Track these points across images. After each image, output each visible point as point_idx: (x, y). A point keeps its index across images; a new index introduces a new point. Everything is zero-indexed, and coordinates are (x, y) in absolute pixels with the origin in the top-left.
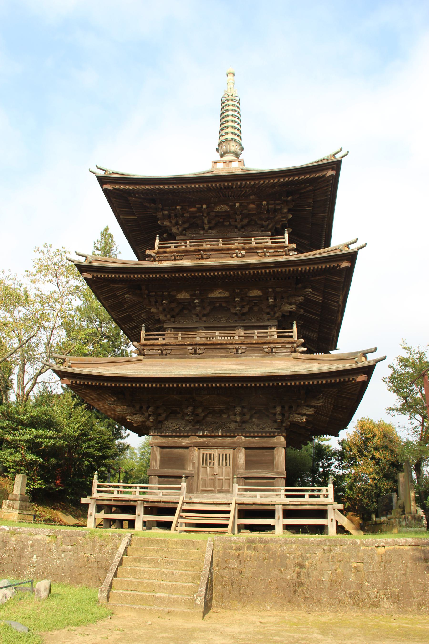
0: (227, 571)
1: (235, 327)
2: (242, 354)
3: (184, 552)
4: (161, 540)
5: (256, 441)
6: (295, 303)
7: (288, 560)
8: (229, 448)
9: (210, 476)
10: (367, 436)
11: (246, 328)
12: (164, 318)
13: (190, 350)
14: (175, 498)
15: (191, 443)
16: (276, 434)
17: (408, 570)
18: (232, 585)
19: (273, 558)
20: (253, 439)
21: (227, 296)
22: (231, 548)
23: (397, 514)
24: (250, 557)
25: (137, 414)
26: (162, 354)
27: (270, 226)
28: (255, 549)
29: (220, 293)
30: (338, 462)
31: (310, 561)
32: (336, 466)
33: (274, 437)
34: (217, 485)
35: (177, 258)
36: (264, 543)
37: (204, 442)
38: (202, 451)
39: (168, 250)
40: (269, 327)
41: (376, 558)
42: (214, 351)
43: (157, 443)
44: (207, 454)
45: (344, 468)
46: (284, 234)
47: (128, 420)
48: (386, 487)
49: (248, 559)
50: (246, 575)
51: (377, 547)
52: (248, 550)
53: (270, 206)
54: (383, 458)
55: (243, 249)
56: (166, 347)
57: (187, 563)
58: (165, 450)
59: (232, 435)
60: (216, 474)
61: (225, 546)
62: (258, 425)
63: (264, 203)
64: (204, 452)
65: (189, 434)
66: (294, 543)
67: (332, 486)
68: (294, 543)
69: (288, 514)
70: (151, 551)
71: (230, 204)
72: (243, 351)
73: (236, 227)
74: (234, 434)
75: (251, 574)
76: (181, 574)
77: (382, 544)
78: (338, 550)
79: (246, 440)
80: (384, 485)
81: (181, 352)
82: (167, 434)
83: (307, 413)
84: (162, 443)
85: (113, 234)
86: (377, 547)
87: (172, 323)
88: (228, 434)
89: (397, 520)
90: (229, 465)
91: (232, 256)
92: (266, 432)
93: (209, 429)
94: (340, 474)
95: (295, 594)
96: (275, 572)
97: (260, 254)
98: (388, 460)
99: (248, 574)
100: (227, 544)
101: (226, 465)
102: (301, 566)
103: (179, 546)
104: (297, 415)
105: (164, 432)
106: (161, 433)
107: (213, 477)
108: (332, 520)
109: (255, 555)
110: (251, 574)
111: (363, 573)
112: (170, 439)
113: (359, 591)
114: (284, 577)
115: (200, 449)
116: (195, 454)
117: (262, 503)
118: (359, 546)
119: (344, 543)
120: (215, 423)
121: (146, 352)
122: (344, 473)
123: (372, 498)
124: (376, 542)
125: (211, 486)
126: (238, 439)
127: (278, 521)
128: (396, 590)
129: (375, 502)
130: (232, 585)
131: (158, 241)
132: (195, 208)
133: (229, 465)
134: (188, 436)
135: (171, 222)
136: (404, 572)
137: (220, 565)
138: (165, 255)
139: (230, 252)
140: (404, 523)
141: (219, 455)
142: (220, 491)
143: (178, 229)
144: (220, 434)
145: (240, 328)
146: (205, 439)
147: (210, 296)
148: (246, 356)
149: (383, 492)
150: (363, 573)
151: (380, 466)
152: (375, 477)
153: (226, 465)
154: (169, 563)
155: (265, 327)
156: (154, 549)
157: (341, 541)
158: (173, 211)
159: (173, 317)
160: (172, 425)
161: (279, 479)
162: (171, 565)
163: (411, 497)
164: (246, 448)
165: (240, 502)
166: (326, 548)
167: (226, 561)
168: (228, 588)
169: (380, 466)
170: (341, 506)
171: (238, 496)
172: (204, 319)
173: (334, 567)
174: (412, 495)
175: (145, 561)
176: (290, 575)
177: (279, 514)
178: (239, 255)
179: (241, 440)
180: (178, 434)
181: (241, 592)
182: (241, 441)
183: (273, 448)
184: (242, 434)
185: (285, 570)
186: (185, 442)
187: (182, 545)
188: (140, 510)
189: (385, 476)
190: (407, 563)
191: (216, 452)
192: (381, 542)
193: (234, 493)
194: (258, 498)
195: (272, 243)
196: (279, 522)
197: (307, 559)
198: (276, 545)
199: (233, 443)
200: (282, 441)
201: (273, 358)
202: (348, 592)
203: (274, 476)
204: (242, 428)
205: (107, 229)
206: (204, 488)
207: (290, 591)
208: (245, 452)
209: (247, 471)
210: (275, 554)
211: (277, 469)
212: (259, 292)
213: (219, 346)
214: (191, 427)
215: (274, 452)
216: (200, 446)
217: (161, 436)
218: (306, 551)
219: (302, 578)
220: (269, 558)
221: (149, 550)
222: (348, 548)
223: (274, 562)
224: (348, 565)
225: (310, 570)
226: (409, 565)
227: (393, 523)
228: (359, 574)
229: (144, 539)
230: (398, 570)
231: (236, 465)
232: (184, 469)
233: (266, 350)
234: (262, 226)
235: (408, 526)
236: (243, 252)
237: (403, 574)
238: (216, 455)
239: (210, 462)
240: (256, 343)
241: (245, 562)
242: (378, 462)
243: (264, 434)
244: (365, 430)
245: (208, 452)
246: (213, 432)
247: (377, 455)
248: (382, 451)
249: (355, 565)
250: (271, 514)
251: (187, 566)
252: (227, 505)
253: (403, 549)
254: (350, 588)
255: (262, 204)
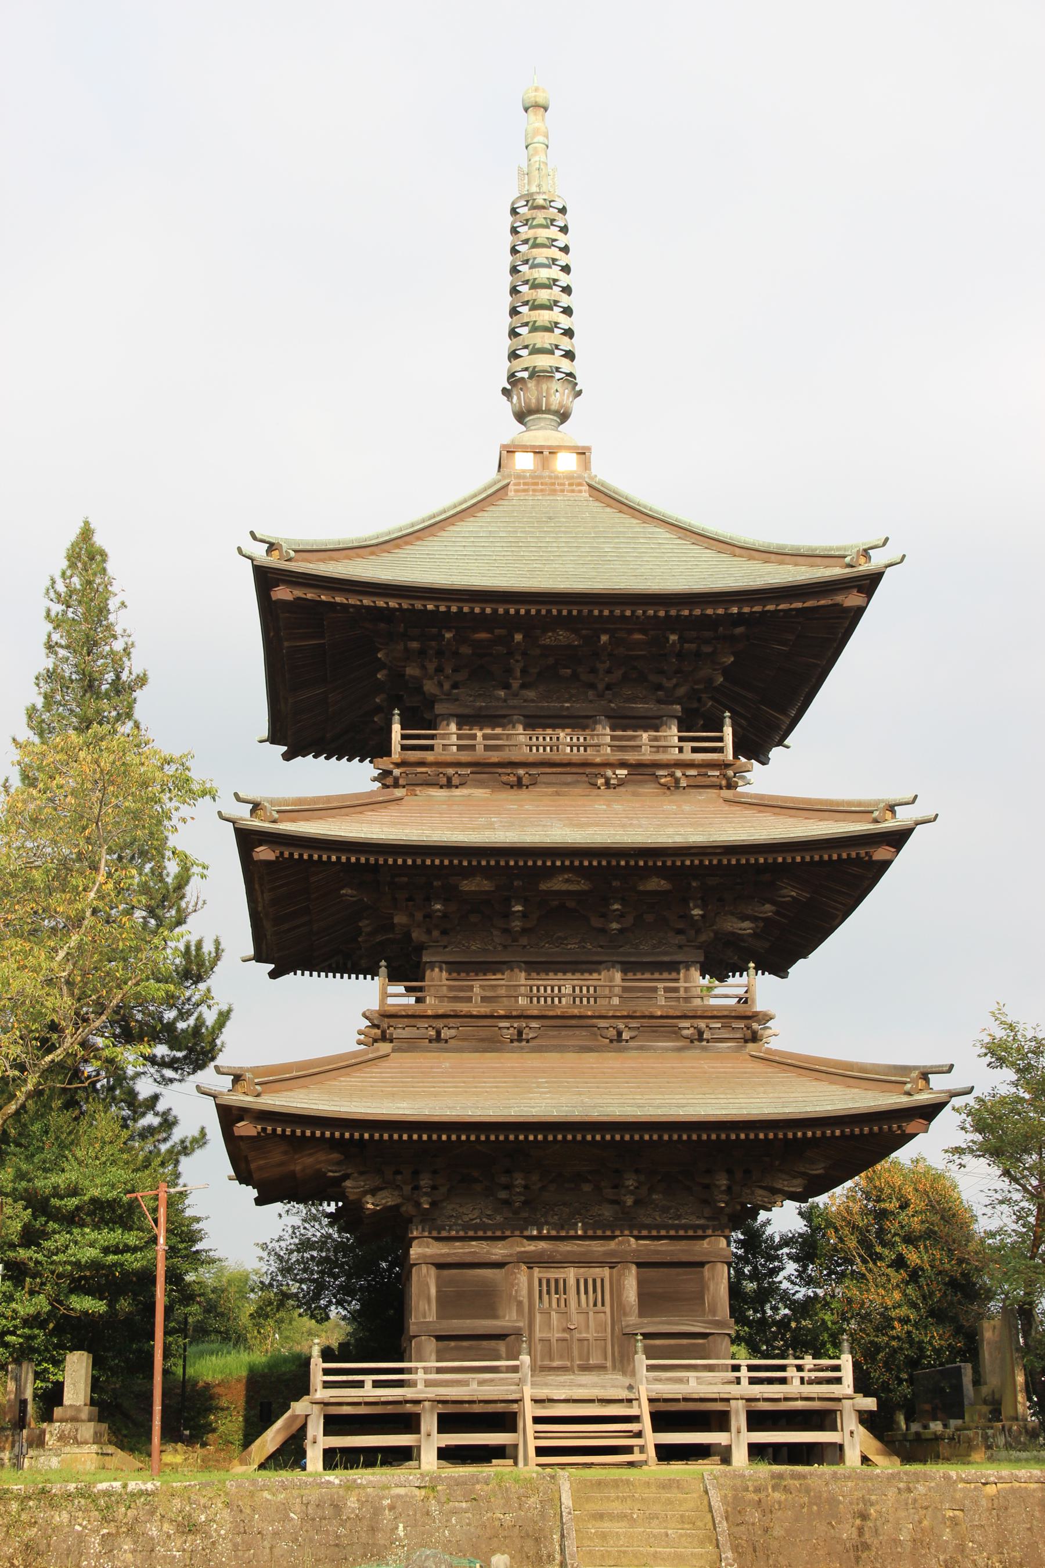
0: (743, 1528)
1: (600, 963)
2: (631, 1044)
3: (669, 1499)
4: (622, 1481)
5: (664, 1248)
6: (754, 919)
7: (841, 1506)
8: (601, 1264)
9: (558, 1332)
10: (886, 1205)
11: (627, 967)
12: (424, 938)
13: (505, 1031)
14: (507, 1390)
15: (511, 1255)
16: (709, 1232)
17: (1035, 1523)
18: (755, 1551)
19: (816, 1504)
20: (656, 1243)
21: (585, 888)
22: (746, 1489)
23: (980, 1418)
24: (780, 1503)
25: (381, 1189)
26: (438, 1038)
27: (681, 691)
28: (786, 1489)
29: (567, 881)
30: (796, 1266)
31: (878, 1507)
32: (793, 1278)
33: (703, 1238)
34: (576, 1353)
35: (456, 781)
36: (799, 1479)
37: (542, 1253)
38: (537, 1272)
39: (429, 756)
40: (681, 966)
41: (984, 1502)
42: (563, 1033)
43: (431, 1256)
44: (548, 1281)
45: (809, 1282)
46: (723, 727)
47: (370, 1206)
48: (937, 1343)
49: (777, 1507)
50: (775, 1534)
51: (984, 1484)
52: (773, 1490)
53: (686, 645)
54: (927, 1267)
55: (623, 765)
56: (446, 1021)
57: (682, 1516)
58: (446, 1272)
59: (608, 1233)
60: (572, 1327)
61: (735, 1485)
62: (665, 1210)
63: (673, 638)
64: (541, 1275)
65: (508, 1233)
66: (849, 1477)
67: (850, 1357)
68: (849, 1477)
69: (758, 1420)
70: (613, 1501)
71: (584, 632)
72: (633, 1034)
73: (592, 686)
74: (613, 1232)
75: (782, 1532)
76: (681, 1536)
77: (992, 1479)
78: (921, 1488)
79: (638, 1245)
80: (933, 1337)
81: (484, 1033)
82: (453, 1233)
83: (786, 1189)
84: (442, 1255)
85: (109, 555)
86: (984, 1484)
87: (441, 949)
88: (599, 1233)
89: (980, 1432)
90: (603, 1305)
91: (593, 781)
92: (685, 1227)
93: (550, 1220)
94: (799, 1296)
95: (858, 1562)
96: (821, 1528)
97: (663, 781)
98: (940, 1273)
99: (778, 1532)
100: (738, 1482)
101: (595, 1305)
102: (864, 1516)
103: (654, 1490)
104: (761, 1192)
105: (444, 1229)
106: (439, 1233)
107: (566, 1335)
108: (852, 1433)
109: (786, 1500)
110: (782, 1532)
111: (964, 1526)
112: (457, 1244)
113: (959, 1557)
114: (837, 1535)
115: (531, 1268)
116: (523, 1281)
117: (702, 1396)
118: (955, 1482)
119: (931, 1477)
120: (564, 1204)
121: (397, 1033)
122: (812, 1295)
123: (899, 1371)
124: (983, 1476)
125: (561, 1358)
126: (620, 1243)
127: (738, 1437)
128: (1017, 1554)
129: (906, 1380)
130: (755, 1551)
131: (399, 726)
132: (492, 633)
133: (603, 1305)
134: (503, 1238)
135: (423, 667)
136: (1028, 1526)
137: (731, 1519)
138: (420, 770)
139: (588, 770)
140: (1001, 1441)
141: (578, 1281)
142: (586, 1368)
143: (440, 685)
144: (580, 1232)
145: (613, 967)
146: (542, 1245)
147: (543, 887)
148: (641, 1048)
149: (930, 1356)
150: (964, 1526)
151: (920, 1287)
152: (908, 1317)
153: (595, 1305)
154: (653, 1518)
155: (673, 967)
156: (618, 1497)
157: (925, 1474)
158: (433, 643)
159: (444, 932)
160: (461, 1210)
161: (719, 1339)
162: (656, 1522)
163: (1018, 1383)
164: (639, 1265)
165: (654, 1395)
166: (902, 1485)
167: (739, 1512)
168: (749, 1558)
169: (920, 1287)
170: (870, 1403)
171: (649, 1384)
172: (524, 941)
173: (916, 1517)
174: (1020, 1379)
175: (612, 1517)
176: (847, 1532)
177: (739, 1420)
178: (612, 782)
179: (629, 1245)
180: (480, 1233)
181: (771, 1562)
182: (628, 1249)
183: (702, 1264)
184: (631, 1232)
185: (839, 1523)
186: (498, 1251)
187: (659, 1486)
188: (429, 1423)
189: (932, 1313)
190: (1033, 1510)
191: (571, 1274)
192: (990, 1475)
193: (638, 1376)
194: (697, 1384)
195: (695, 750)
196: (739, 1439)
197: (872, 1504)
198: (820, 1482)
199: (612, 1253)
200: (722, 1249)
201: (704, 1054)
202: (941, 1558)
203: (708, 1331)
204: (627, 1221)
205: (86, 534)
206: (546, 1363)
207: (849, 1558)
208: (638, 1273)
209: (645, 1320)
210: (820, 1497)
211: (714, 1314)
212: (663, 882)
213: (573, 1022)
214: (511, 1215)
215: (702, 1273)
216: (531, 1262)
217: (437, 1239)
218: (870, 1492)
219: (867, 1536)
220: (811, 1504)
221: (608, 1498)
222: (937, 1485)
223: (819, 1511)
224: (939, 1514)
225: (878, 1523)
226: (1037, 1514)
227: (969, 1441)
228: (958, 1528)
229: (591, 1481)
230: (1019, 1523)
231: (619, 1307)
232: (495, 1317)
233: (685, 1032)
234: (659, 687)
235: (1014, 1449)
236: (622, 772)
237: (1029, 1529)
238: (572, 1282)
239: (558, 1300)
240: (661, 1017)
241: (771, 1512)
242: (915, 1275)
243: (681, 1233)
244: (881, 1190)
245: (553, 1274)
246: (562, 1228)
247: (913, 1257)
248: (925, 1247)
249: (950, 1513)
250: (719, 1421)
251: (683, 1522)
252: (625, 1404)
253: (1026, 1488)
254: (945, 1552)
255: (668, 639)
